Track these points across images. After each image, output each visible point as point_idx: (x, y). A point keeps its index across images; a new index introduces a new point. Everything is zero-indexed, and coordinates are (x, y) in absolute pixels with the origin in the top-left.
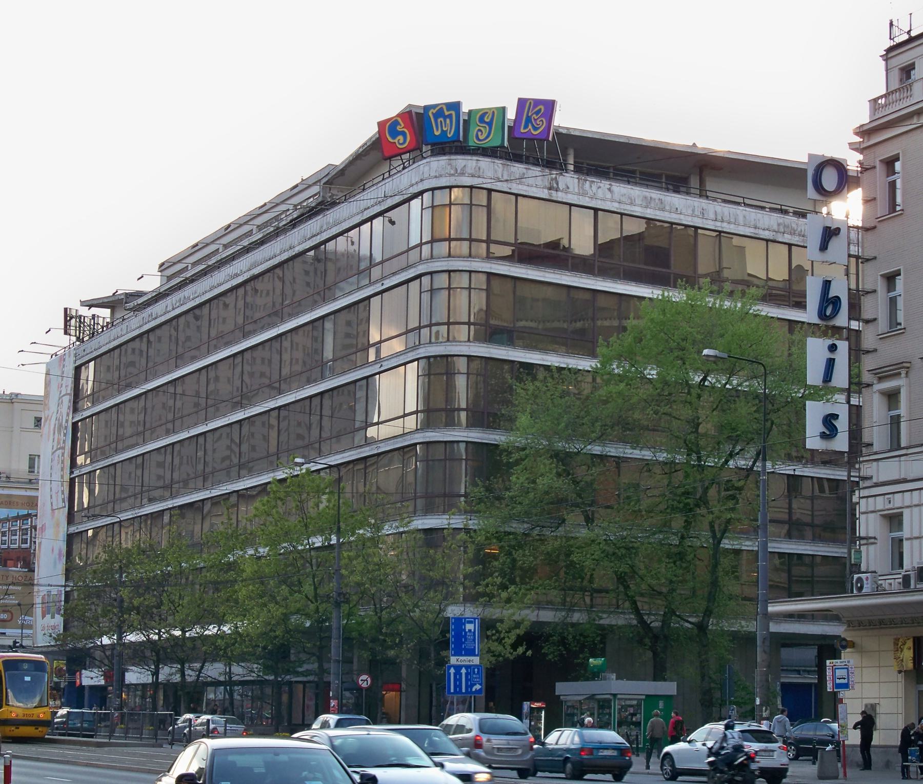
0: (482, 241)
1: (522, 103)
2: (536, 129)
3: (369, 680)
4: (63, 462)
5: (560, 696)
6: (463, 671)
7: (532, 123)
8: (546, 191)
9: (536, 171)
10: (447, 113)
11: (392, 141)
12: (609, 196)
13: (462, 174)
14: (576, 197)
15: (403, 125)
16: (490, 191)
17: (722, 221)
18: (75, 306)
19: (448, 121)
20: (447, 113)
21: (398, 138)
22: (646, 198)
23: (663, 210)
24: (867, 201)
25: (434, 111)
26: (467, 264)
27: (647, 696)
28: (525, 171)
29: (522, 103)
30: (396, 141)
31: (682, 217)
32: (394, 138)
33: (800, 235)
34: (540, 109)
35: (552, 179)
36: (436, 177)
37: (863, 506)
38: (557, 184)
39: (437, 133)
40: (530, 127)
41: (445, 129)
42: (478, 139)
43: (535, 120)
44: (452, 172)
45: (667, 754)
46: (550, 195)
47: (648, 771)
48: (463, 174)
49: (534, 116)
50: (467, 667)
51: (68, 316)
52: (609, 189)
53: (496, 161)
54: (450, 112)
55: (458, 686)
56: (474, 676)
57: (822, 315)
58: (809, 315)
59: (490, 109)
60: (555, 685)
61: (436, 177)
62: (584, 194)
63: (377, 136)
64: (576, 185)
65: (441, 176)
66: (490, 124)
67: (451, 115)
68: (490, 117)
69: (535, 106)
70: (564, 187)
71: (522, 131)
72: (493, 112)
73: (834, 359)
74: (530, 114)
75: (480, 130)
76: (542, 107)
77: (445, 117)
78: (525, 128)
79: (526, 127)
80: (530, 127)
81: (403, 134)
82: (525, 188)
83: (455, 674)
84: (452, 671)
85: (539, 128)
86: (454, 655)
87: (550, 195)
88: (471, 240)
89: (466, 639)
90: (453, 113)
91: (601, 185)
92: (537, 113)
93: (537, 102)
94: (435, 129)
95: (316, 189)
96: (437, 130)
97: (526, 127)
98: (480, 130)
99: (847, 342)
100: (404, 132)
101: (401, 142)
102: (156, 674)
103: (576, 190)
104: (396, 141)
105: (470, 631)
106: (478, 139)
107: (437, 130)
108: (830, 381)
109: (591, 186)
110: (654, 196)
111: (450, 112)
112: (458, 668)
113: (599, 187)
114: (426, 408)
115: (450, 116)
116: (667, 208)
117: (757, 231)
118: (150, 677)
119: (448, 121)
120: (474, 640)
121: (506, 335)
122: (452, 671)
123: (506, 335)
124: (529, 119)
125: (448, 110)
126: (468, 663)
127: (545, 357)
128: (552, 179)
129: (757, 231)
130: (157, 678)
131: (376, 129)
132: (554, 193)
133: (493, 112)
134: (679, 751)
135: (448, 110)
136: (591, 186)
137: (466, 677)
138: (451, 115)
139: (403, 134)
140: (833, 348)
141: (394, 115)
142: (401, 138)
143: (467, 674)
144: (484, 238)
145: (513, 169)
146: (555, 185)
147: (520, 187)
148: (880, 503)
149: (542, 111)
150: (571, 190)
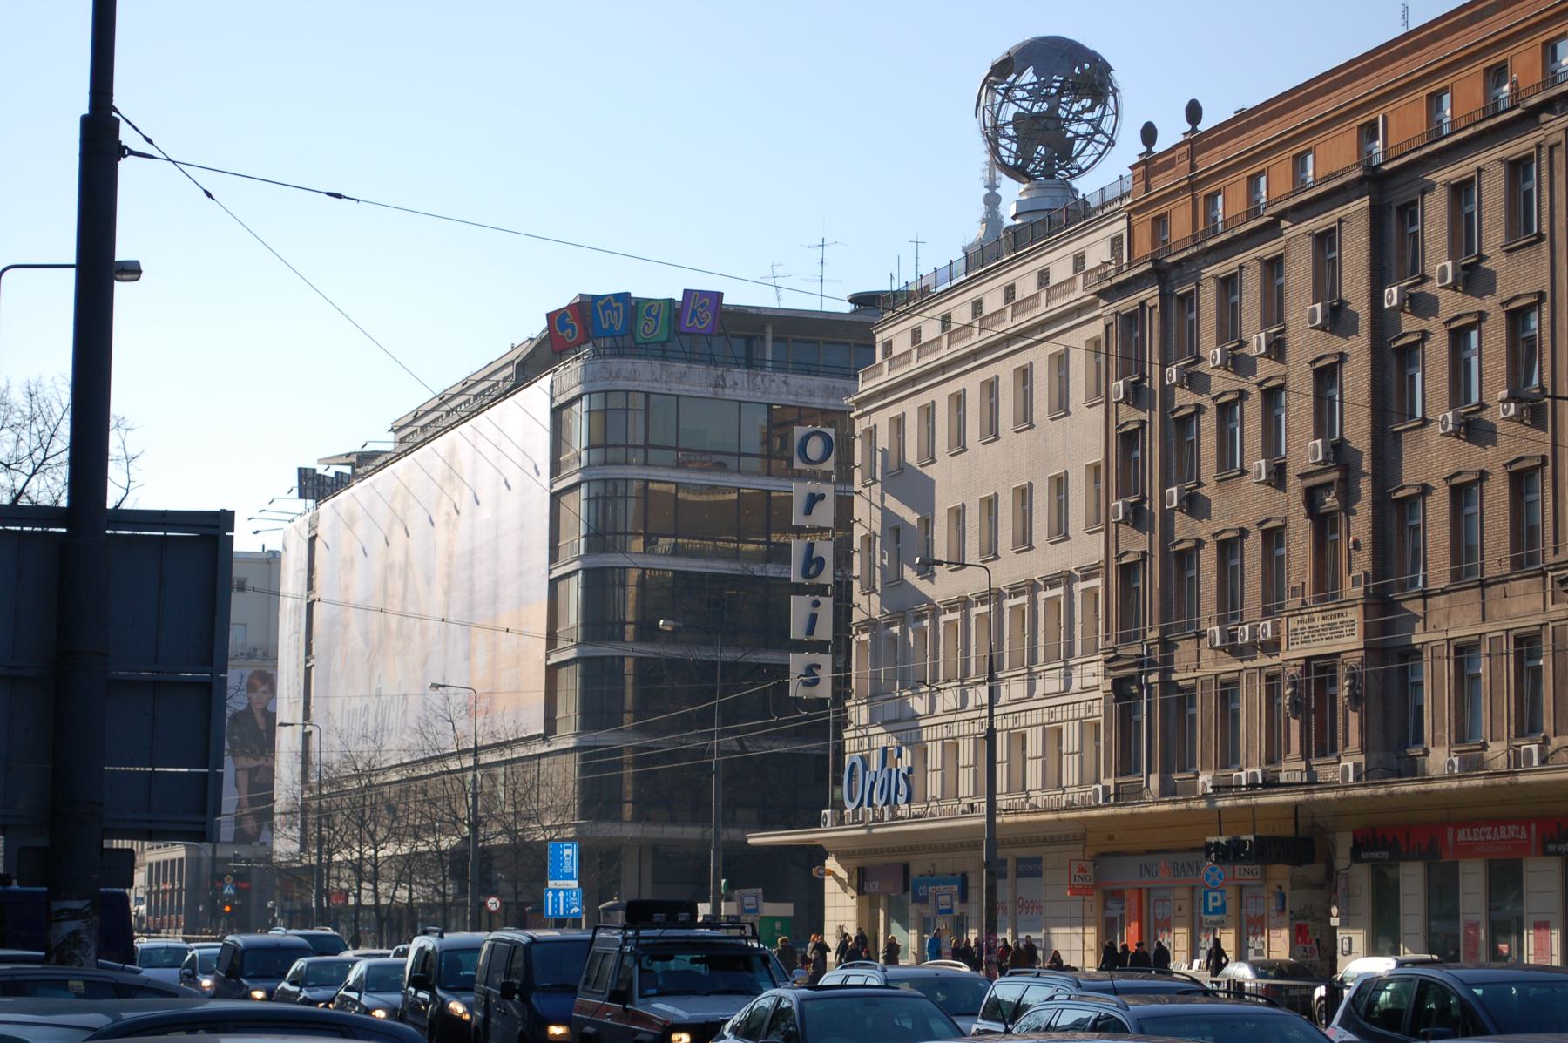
0: (639, 447)
2: (701, 323)
6: (561, 894)
8: (711, 389)
9: (698, 370)
10: (614, 305)
12: (784, 389)
13: (617, 377)
14: (745, 393)
16: (647, 394)
18: (310, 464)
19: (615, 313)
20: (614, 305)
22: (827, 387)
26: (623, 471)
28: (686, 370)
30: (565, 334)
32: (563, 331)
35: (718, 377)
37: (135, 842)
38: (724, 381)
39: (605, 326)
40: (696, 321)
42: (646, 334)
46: (716, 393)
50: (565, 890)
51: (304, 474)
52: (785, 382)
53: (654, 362)
57: (806, 574)
58: (795, 576)
60: (795, 912)
62: (756, 388)
64: (746, 380)
66: (657, 317)
70: (731, 383)
71: (688, 325)
73: (817, 615)
75: (646, 324)
76: (707, 300)
77: (613, 310)
79: (691, 321)
80: (696, 321)
81: (572, 327)
82: (687, 388)
83: (553, 898)
84: (550, 894)
86: (552, 879)
87: (716, 393)
88: (627, 446)
89: (564, 865)
91: (775, 378)
92: (702, 306)
95: (510, 370)
97: (691, 321)
98: (646, 324)
101: (570, 335)
103: (746, 386)
104: (565, 334)
105: (568, 856)
106: (646, 334)
108: (812, 634)
109: (763, 381)
110: (836, 385)
112: (556, 892)
115: (617, 309)
119: (615, 313)
120: (572, 865)
122: (550, 894)
125: (616, 302)
127: (710, 564)
128: (718, 377)
131: (544, 324)
132: (720, 390)
136: (763, 381)
139: (572, 327)
140: (816, 604)
142: (569, 331)
143: (565, 898)
144: (642, 444)
145: (673, 369)
146: (721, 382)
147: (682, 387)
148: (943, 732)
150: (740, 385)
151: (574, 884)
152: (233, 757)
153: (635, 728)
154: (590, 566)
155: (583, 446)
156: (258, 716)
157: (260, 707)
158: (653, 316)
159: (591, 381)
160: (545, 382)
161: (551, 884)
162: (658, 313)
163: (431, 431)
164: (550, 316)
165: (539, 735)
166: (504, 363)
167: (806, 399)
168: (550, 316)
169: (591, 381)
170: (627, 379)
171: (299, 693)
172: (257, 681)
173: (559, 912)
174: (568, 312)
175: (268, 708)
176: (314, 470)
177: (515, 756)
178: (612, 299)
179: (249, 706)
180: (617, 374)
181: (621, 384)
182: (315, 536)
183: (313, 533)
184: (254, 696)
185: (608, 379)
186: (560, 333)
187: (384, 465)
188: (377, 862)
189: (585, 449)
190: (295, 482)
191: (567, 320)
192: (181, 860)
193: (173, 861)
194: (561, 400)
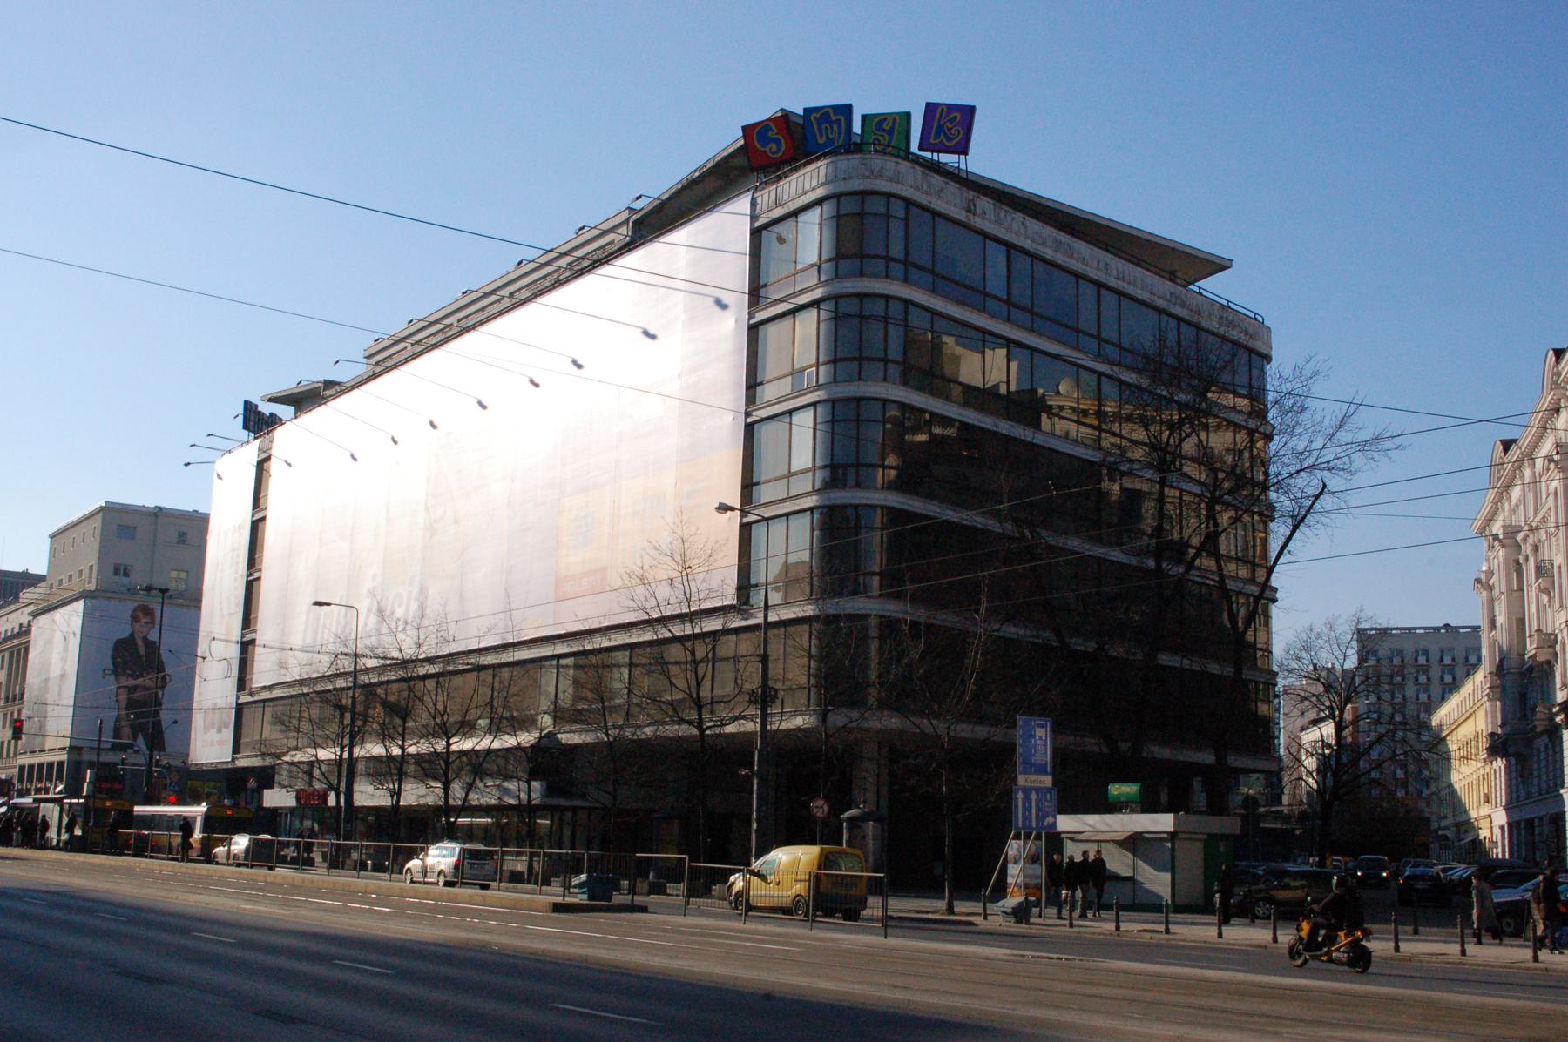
1: (931, 108)
2: (950, 139)
3: (826, 808)
4: (237, 564)
5: (1060, 833)
6: (1033, 796)
7: (945, 134)
8: (964, 213)
10: (833, 118)
13: (880, 176)
15: (776, 131)
17: (1124, 281)
18: (255, 400)
19: (835, 128)
20: (833, 118)
21: (769, 146)
23: (1071, 257)
25: (818, 115)
27: (1209, 835)
28: (944, 185)
29: (931, 108)
30: (767, 149)
31: (1088, 268)
33: (1188, 309)
34: (955, 117)
38: (975, 206)
40: (942, 137)
41: (830, 136)
43: (950, 129)
44: (867, 174)
45: (409, 869)
47: (1221, 940)
49: (948, 124)
51: (249, 407)
54: (837, 117)
55: (1027, 818)
56: (1046, 804)
63: (742, 142)
66: (890, 132)
67: (839, 120)
69: (948, 113)
71: (932, 141)
72: (895, 118)
77: (831, 123)
80: (942, 137)
81: (777, 141)
89: (1036, 751)
90: (843, 118)
92: (951, 121)
93: (952, 108)
94: (818, 136)
96: (821, 136)
100: (778, 139)
101: (774, 149)
102: (397, 793)
107: (821, 136)
111: (837, 117)
112: (1027, 791)
113: (1013, 219)
114: (829, 463)
116: (1075, 255)
117: (1153, 297)
118: (390, 799)
119: (835, 128)
122: (1020, 796)
124: (940, 129)
125: (835, 115)
126: (1039, 785)
129: (1153, 297)
130: (398, 801)
132: (971, 216)
134: (414, 865)
135: (835, 115)
137: (1037, 806)
138: (839, 120)
141: (765, 118)
149: (958, 119)
151: (1047, 781)
152: (116, 676)
153: (880, 595)
154: (836, 396)
155: (824, 258)
156: (140, 643)
157: (141, 635)
158: (884, 131)
159: (844, 179)
160: (742, 204)
161: (1022, 780)
162: (893, 128)
163: (388, 364)
164: (747, 130)
165: (732, 607)
166: (589, 237)
167: (1039, 247)
168: (747, 130)
169: (844, 179)
170: (891, 180)
171: (237, 605)
172: (141, 615)
173: (1030, 822)
174: (771, 124)
175: (148, 637)
176: (256, 406)
177: (697, 630)
178: (831, 111)
179: (132, 635)
180: (880, 171)
181: (884, 186)
182: (268, 459)
183: (264, 456)
184: (137, 626)
185: (867, 177)
186: (758, 146)
187: (343, 392)
188: (448, 758)
189: (830, 260)
190: (241, 410)
191: (770, 133)
192: (61, 764)
193: (51, 765)
194: (762, 221)
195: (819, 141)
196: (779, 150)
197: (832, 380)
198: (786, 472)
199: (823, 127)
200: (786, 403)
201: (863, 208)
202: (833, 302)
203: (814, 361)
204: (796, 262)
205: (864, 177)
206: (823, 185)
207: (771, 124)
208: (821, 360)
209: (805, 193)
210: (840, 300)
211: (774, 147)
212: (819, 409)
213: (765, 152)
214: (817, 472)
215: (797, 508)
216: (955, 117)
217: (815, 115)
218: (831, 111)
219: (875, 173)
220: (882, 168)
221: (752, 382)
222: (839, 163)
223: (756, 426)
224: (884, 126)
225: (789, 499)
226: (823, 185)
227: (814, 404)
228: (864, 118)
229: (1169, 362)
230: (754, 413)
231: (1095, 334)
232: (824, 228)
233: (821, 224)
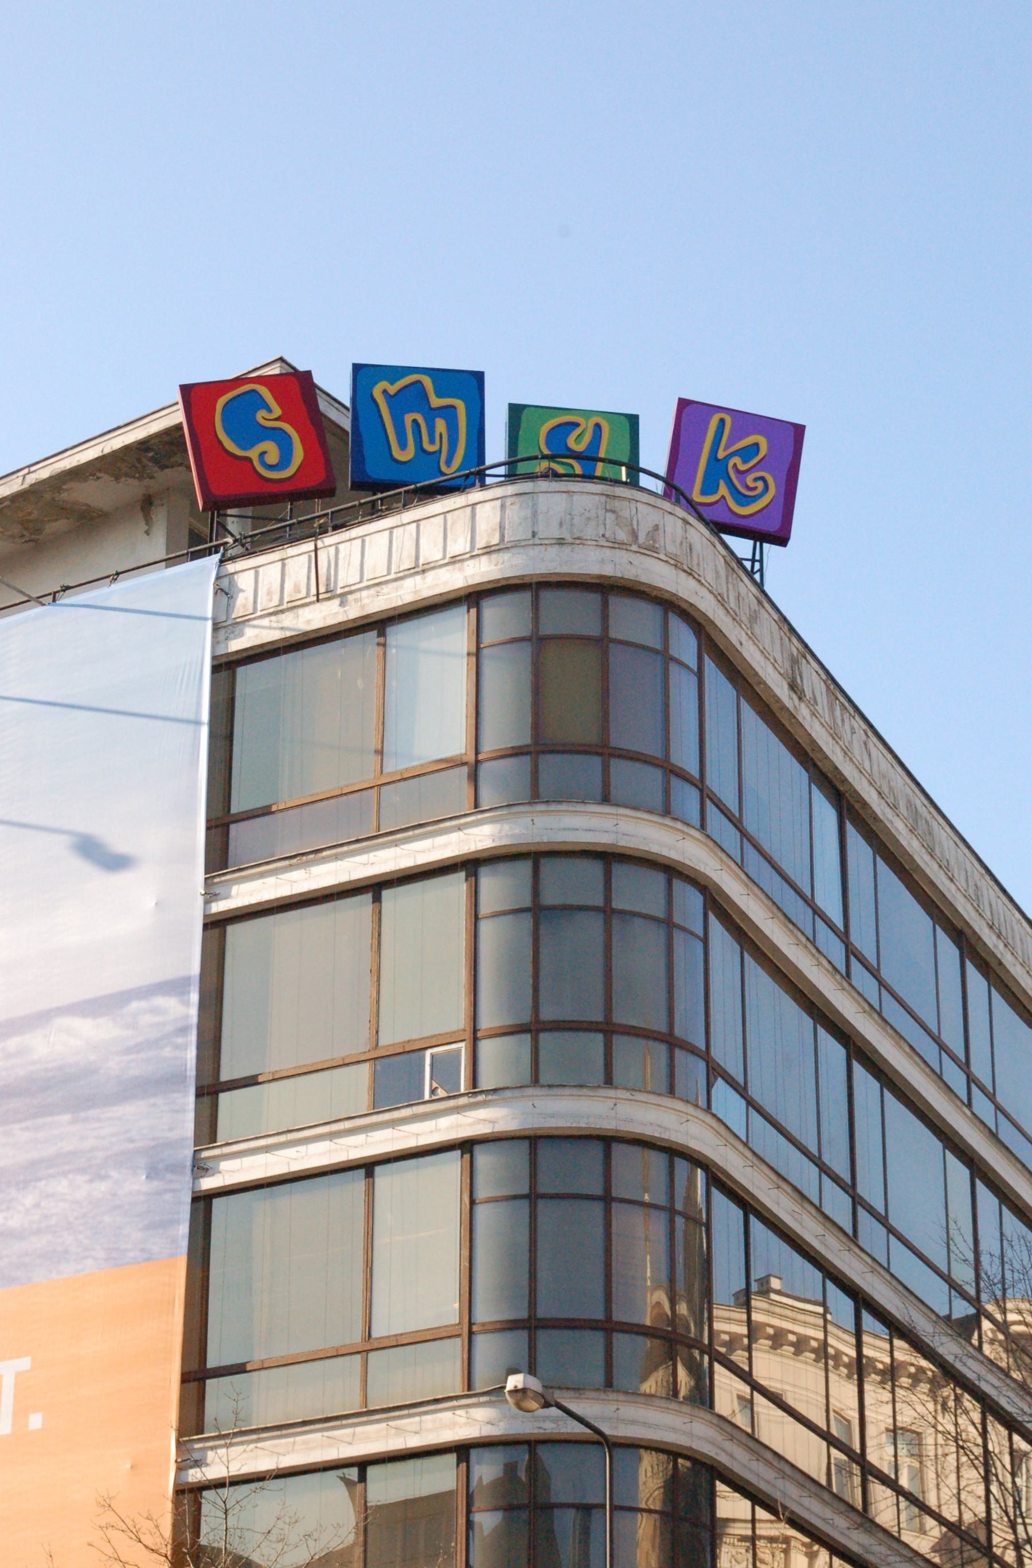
2: (744, 500)
10: (436, 402)
11: (239, 453)
13: (651, 549)
15: (278, 412)
19: (441, 426)
20: (436, 402)
24: (700, 1050)
25: (393, 389)
30: (253, 454)
34: (756, 446)
36: (560, 542)
39: (407, 455)
40: (723, 490)
44: (622, 536)
48: (654, 549)
49: (736, 460)
59: (587, 414)
61: (560, 542)
65: (579, 541)
68: (587, 438)
72: (598, 426)
74: (721, 454)
77: (432, 414)
78: (704, 492)
80: (723, 490)
85: (755, 499)
96: (403, 446)
99: (208, 1382)
101: (273, 458)
107: (403, 445)
115: (448, 412)
119: (441, 426)
121: (202, 1202)
123: (202, 1202)
124: (717, 468)
125: (439, 395)
133: (598, 426)
149: (764, 450)
195: (764, 450)
196: (285, 460)
197: (527, 1077)
198: (356, 1337)
199: (409, 418)
200: (359, 1139)
201: (605, 628)
202: (525, 868)
203: (458, 1020)
204: (380, 752)
205: (617, 545)
206: (489, 550)
207: (264, 391)
208: (487, 1022)
209: (420, 569)
210: (547, 866)
211: (272, 451)
212: (484, 1159)
213: (249, 460)
214: (482, 1342)
215: (414, 1442)
216: (756, 446)
217: (383, 385)
218: (427, 382)
219: (642, 539)
220: (656, 528)
221: (208, 1081)
222: (542, 498)
223: (216, 1202)
224: (571, 443)
225: (367, 1414)
226: (489, 550)
227: (467, 1146)
228: (516, 411)
229: (65, 1182)
230: (224, 1165)
231: (678, 1053)
232: (489, 669)
233: (477, 654)
